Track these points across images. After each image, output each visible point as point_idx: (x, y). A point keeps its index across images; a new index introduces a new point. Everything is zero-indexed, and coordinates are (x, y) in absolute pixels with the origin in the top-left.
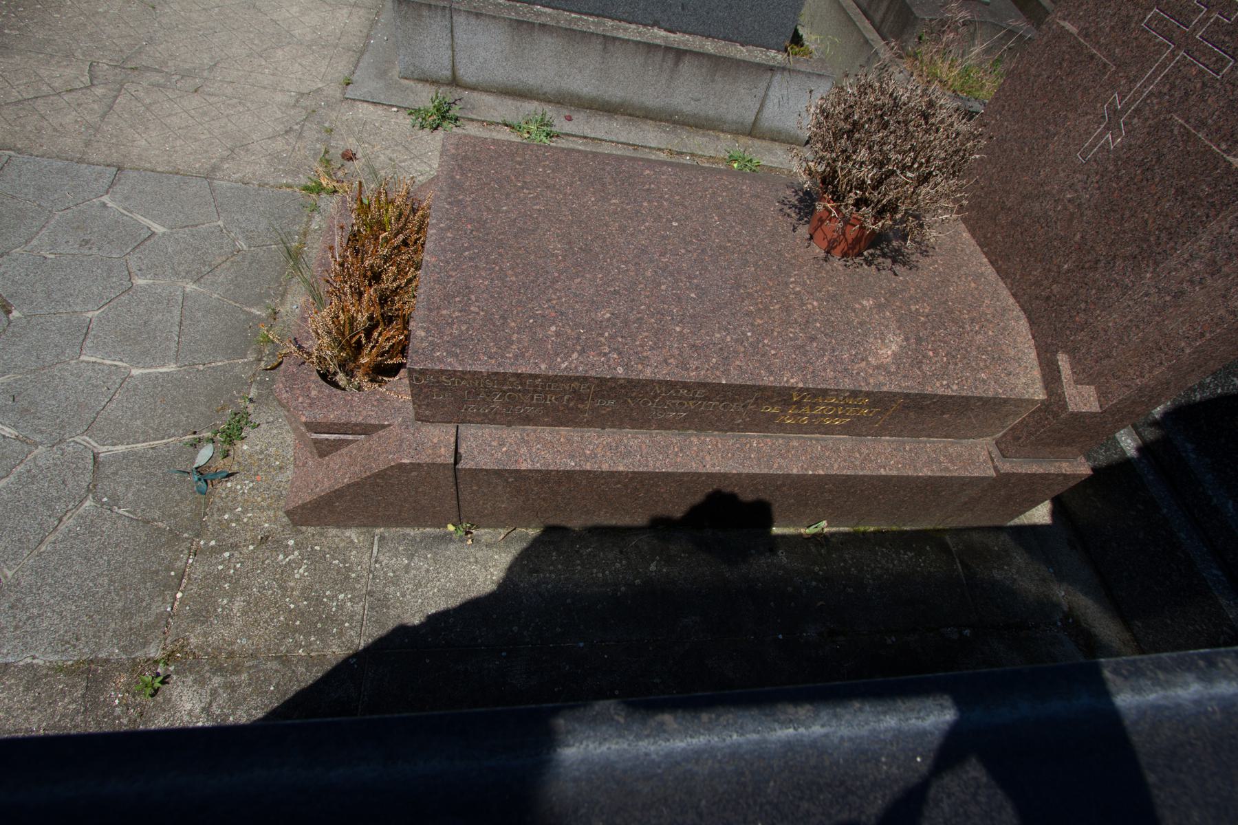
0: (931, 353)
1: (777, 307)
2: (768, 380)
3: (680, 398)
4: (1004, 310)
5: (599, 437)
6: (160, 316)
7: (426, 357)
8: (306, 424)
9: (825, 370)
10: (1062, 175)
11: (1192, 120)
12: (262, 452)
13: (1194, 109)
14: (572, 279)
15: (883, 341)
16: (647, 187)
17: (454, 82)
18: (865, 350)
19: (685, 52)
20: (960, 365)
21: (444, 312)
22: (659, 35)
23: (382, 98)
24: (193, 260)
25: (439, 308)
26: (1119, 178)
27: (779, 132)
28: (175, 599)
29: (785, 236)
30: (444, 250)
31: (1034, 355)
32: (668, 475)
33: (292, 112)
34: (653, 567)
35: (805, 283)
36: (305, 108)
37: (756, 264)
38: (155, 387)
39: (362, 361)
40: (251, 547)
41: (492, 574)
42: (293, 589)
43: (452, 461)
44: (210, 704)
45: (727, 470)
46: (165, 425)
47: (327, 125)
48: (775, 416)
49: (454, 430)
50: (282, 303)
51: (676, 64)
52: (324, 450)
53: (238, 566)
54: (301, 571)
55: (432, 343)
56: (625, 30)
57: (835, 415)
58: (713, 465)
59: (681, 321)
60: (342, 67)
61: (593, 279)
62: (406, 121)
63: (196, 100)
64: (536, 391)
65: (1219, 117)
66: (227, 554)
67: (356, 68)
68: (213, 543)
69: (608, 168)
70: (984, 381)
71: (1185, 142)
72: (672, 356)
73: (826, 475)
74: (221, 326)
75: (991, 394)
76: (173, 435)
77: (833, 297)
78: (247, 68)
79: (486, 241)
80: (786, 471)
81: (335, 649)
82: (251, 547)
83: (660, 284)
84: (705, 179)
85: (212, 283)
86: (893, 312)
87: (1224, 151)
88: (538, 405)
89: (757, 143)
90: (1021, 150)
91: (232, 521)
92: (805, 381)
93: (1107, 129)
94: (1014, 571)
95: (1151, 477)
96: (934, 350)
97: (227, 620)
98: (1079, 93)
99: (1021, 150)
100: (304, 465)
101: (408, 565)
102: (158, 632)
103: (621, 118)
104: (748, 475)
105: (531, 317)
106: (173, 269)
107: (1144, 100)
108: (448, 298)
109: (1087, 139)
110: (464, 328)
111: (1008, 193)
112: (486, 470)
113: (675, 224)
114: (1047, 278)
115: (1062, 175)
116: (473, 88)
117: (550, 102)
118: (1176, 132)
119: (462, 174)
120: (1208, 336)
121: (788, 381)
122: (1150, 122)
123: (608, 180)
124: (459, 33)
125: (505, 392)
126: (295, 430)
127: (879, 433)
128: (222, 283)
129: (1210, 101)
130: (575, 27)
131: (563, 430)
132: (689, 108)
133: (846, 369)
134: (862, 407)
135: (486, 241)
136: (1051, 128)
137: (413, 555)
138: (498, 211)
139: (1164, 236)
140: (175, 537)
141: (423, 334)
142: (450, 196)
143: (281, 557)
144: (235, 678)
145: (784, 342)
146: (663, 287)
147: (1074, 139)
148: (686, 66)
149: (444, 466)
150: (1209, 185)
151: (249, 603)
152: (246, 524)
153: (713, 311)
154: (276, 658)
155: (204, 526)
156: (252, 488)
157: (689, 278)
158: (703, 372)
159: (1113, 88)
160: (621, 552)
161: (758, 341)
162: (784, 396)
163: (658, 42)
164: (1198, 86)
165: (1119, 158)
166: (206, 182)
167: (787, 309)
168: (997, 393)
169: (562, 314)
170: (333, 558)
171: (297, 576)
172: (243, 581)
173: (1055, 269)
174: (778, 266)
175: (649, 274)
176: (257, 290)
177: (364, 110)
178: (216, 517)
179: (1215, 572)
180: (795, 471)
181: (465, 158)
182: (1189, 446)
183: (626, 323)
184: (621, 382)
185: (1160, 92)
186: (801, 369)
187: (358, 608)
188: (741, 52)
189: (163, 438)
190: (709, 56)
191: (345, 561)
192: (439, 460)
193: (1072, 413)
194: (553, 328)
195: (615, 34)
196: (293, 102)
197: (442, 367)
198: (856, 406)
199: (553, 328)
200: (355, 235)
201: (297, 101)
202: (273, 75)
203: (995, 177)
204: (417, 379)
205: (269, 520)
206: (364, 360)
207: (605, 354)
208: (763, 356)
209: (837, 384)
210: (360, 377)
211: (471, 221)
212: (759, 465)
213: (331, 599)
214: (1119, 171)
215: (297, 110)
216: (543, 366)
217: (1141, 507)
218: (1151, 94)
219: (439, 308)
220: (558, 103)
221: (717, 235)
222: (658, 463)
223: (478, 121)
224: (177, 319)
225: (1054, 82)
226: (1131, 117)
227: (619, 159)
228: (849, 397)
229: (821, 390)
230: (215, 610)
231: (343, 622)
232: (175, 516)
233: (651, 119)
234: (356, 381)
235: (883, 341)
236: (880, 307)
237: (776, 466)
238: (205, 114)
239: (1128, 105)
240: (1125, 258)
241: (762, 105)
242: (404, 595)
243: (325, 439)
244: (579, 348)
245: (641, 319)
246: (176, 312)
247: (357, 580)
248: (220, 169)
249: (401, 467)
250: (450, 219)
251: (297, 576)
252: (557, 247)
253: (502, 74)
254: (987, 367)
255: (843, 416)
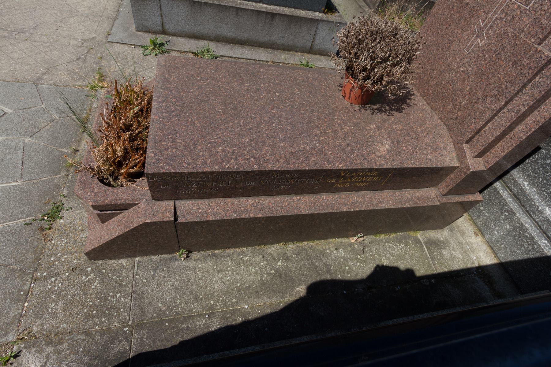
0: (405, 148)
1: (330, 131)
2: (328, 166)
3: (286, 179)
4: (436, 125)
5: (248, 201)
6: (11, 156)
7: (155, 167)
8: (92, 206)
9: (355, 160)
10: (458, 60)
11: (517, 29)
12: (71, 223)
13: (517, 24)
14: (229, 124)
15: (382, 144)
16: (262, 77)
17: (164, 32)
18: (374, 149)
19: (276, 14)
20: (419, 153)
21: (163, 143)
22: (263, 7)
23: (127, 41)
24: (29, 126)
25: (160, 141)
26: (485, 59)
27: (323, 51)
28: (24, 306)
29: (330, 97)
30: (162, 113)
31: (452, 146)
32: (283, 217)
33: (80, 49)
34: (279, 264)
35: (342, 119)
36: (87, 47)
37: (318, 111)
38: (9, 193)
39: (122, 171)
40: (67, 274)
41: (198, 275)
42: (91, 294)
43: (173, 219)
44: (46, 363)
45: (312, 212)
46: (15, 213)
47: (99, 55)
48: (333, 184)
49: (173, 203)
50: (79, 145)
51: (272, 20)
52: (104, 219)
53: (60, 285)
54: (95, 284)
55: (157, 159)
56: (246, 4)
57: (362, 181)
58: (305, 210)
59: (284, 141)
60: (106, 26)
61: (239, 123)
62: (139, 51)
63: (27, 44)
64: (214, 180)
65: (530, 27)
66: (53, 279)
67: (112, 26)
68: (45, 274)
69: (242, 69)
70: (430, 160)
71: (515, 40)
72: (281, 158)
73: (360, 211)
74: (46, 159)
75: (434, 166)
76: (21, 218)
77: (356, 125)
78: (54, 28)
79: (183, 107)
80: (340, 210)
81: (116, 324)
82: (67, 274)
83: (272, 123)
84: (290, 72)
85: (40, 137)
86: (385, 130)
87: (533, 42)
88: (215, 188)
89: (313, 56)
90: (438, 50)
91: (55, 261)
92: (346, 166)
93: (477, 36)
94: (451, 249)
95: (510, 199)
96: (406, 147)
97: (54, 315)
98: (463, 21)
99: (438, 50)
100: (94, 228)
101: (154, 275)
102: (14, 326)
103: (248, 47)
104: (322, 214)
105: (209, 143)
106: (17, 131)
107: (494, 22)
108: (165, 136)
109: (468, 42)
110: (174, 151)
111: (433, 70)
112: (191, 222)
113: (277, 94)
114: (455, 109)
115: (458, 60)
116: (174, 35)
117: (212, 40)
118: (510, 35)
119: (169, 75)
120: (533, 130)
121: (338, 166)
122: (497, 32)
123: (243, 74)
124: (166, 10)
125: (198, 182)
126: (88, 211)
127: (382, 189)
128: (45, 137)
129: (524, 20)
130: (222, 4)
131: (230, 200)
132: (280, 42)
133: (365, 159)
134: (374, 176)
135: (183, 107)
136: (451, 38)
137: (156, 269)
138: (188, 92)
139: (509, 85)
140: (23, 272)
141: (153, 155)
142: (163, 85)
143: (84, 277)
144: (59, 347)
145: (335, 147)
146: (274, 125)
147: (462, 43)
148: (276, 21)
149: (169, 222)
150: (527, 59)
151: (66, 304)
152: (64, 262)
153: (299, 135)
154: (83, 333)
155: (39, 265)
156: (67, 242)
157: (286, 119)
158: (296, 165)
159: (478, 17)
160: (263, 257)
161: (323, 148)
162: (336, 174)
163: (263, 10)
164: (519, 13)
165: (484, 50)
166: (34, 86)
167: (335, 132)
168: (437, 165)
169: (224, 141)
170: (113, 275)
171: (93, 287)
172: (63, 293)
173: (458, 104)
174: (329, 111)
175: (266, 119)
176: (65, 139)
177: (119, 48)
178: (46, 259)
179: (544, 241)
180: (345, 210)
181: (170, 66)
182: (526, 183)
183: (257, 143)
184: (256, 172)
185: (501, 18)
186: (344, 160)
187: (128, 300)
188: (302, 13)
189: (14, 220)
190: (288, 16)
191: (119, 276)
192: (166, 219)
193: (472, 172)
194: (220, 148)
195: (241, 6)
196: (80, 44)
197: (164, 171)
198: (371, 176)
199: (220, 148)
200: (115, 108)
201: (82, 43)
202: (69, 31)
203: (427, 63)
204: (151, 178)
205: (76, 258)
206: (123, 171)
207: (248, 159)
208: (325, 155)
209: (362, 166)
210: (121, 180)
211: (175, 97)
212: (327, 208)
213: (112, 297)
214: (485, 56)
215: (83, 48)
216: (217, 167)
217: (507, 214)
218: (497, 19)
219: (160, 141)
220: (217, 41)
221: (298, 98)
222: (278, 212)
223: (178, 51)
224: (20, 157)
225: (450, 17)
226: (488, 30)
227: (247, 64)
228: (368, 172)
229: (355, 169)
230: (48, 310)
231: (120, 309)
232: (22, 261)
233: (262, 47)
234: (119, 182)
235: (382, 144)
236: (378, 128)
237: (336, 208)
238: (32, 51)
239: (486, 25)
240: (491, 97)
241: (314, 38)
242: (152, 291)
243: (106, 212)
244: (234, 157)
245: (265, 141)
246: (20, 153)
247: (126, 286)
248: (42, 79)
249: (146, 224)
250: (164, 97)
251: (93, 287)
252: (219, 108)
253: (188, 27)
254: (431, 153)
255: (366, 181)
